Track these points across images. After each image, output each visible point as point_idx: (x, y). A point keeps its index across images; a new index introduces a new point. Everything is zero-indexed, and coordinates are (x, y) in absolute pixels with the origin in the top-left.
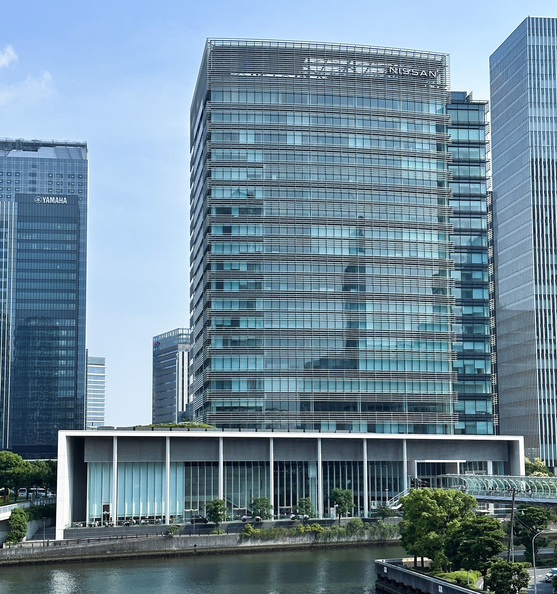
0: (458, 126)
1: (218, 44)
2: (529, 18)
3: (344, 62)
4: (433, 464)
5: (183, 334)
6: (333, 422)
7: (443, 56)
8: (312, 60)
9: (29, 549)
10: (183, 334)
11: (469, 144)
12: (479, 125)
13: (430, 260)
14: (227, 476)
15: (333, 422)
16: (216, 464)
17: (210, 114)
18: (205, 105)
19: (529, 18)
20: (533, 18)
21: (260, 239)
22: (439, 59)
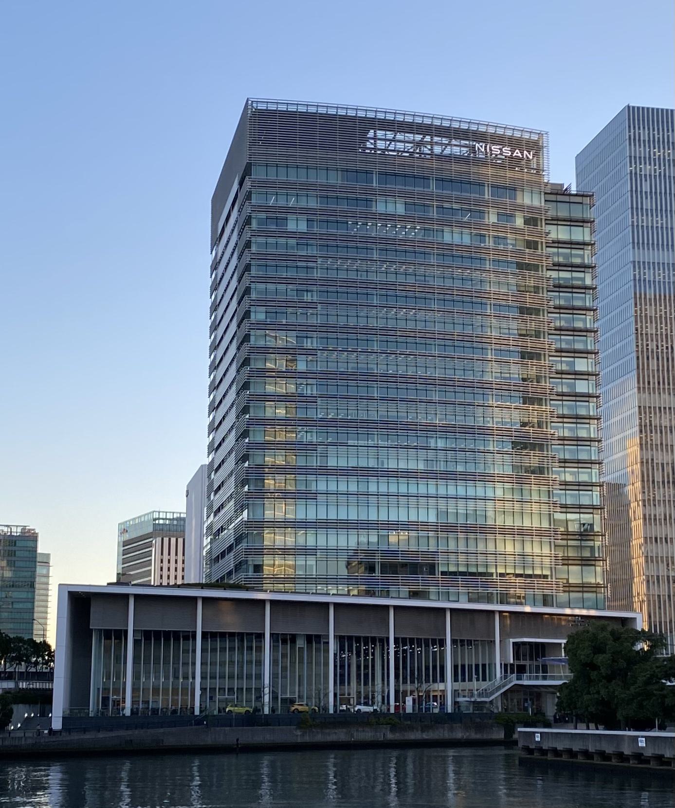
0: (556, 221)
1: (262, 107)
2: (629, 107)
3: (418, 138)
4: (536, 643)
5: (159, 519)
6: (406, 589)
7: (540, 134)
8: (380, 134)
9: (20, 738)
10: (159, 519)
11: (572, 244)
12: (584, 222)
13: (426, 524)
14: (274, 648)
15: (406, 589)
16: (260, 636)
17: (250, 193)
18: (241, 184)
19: (629, 107)
20: (634, 108)
21: (313, 352)
22: (535, 137)
